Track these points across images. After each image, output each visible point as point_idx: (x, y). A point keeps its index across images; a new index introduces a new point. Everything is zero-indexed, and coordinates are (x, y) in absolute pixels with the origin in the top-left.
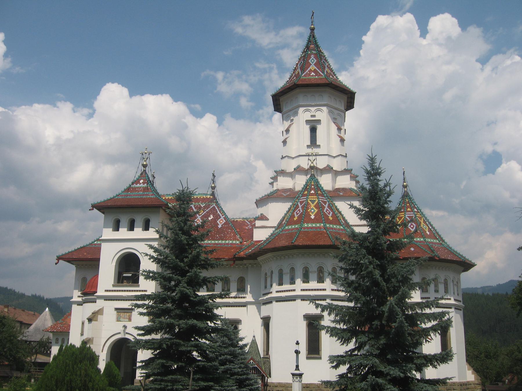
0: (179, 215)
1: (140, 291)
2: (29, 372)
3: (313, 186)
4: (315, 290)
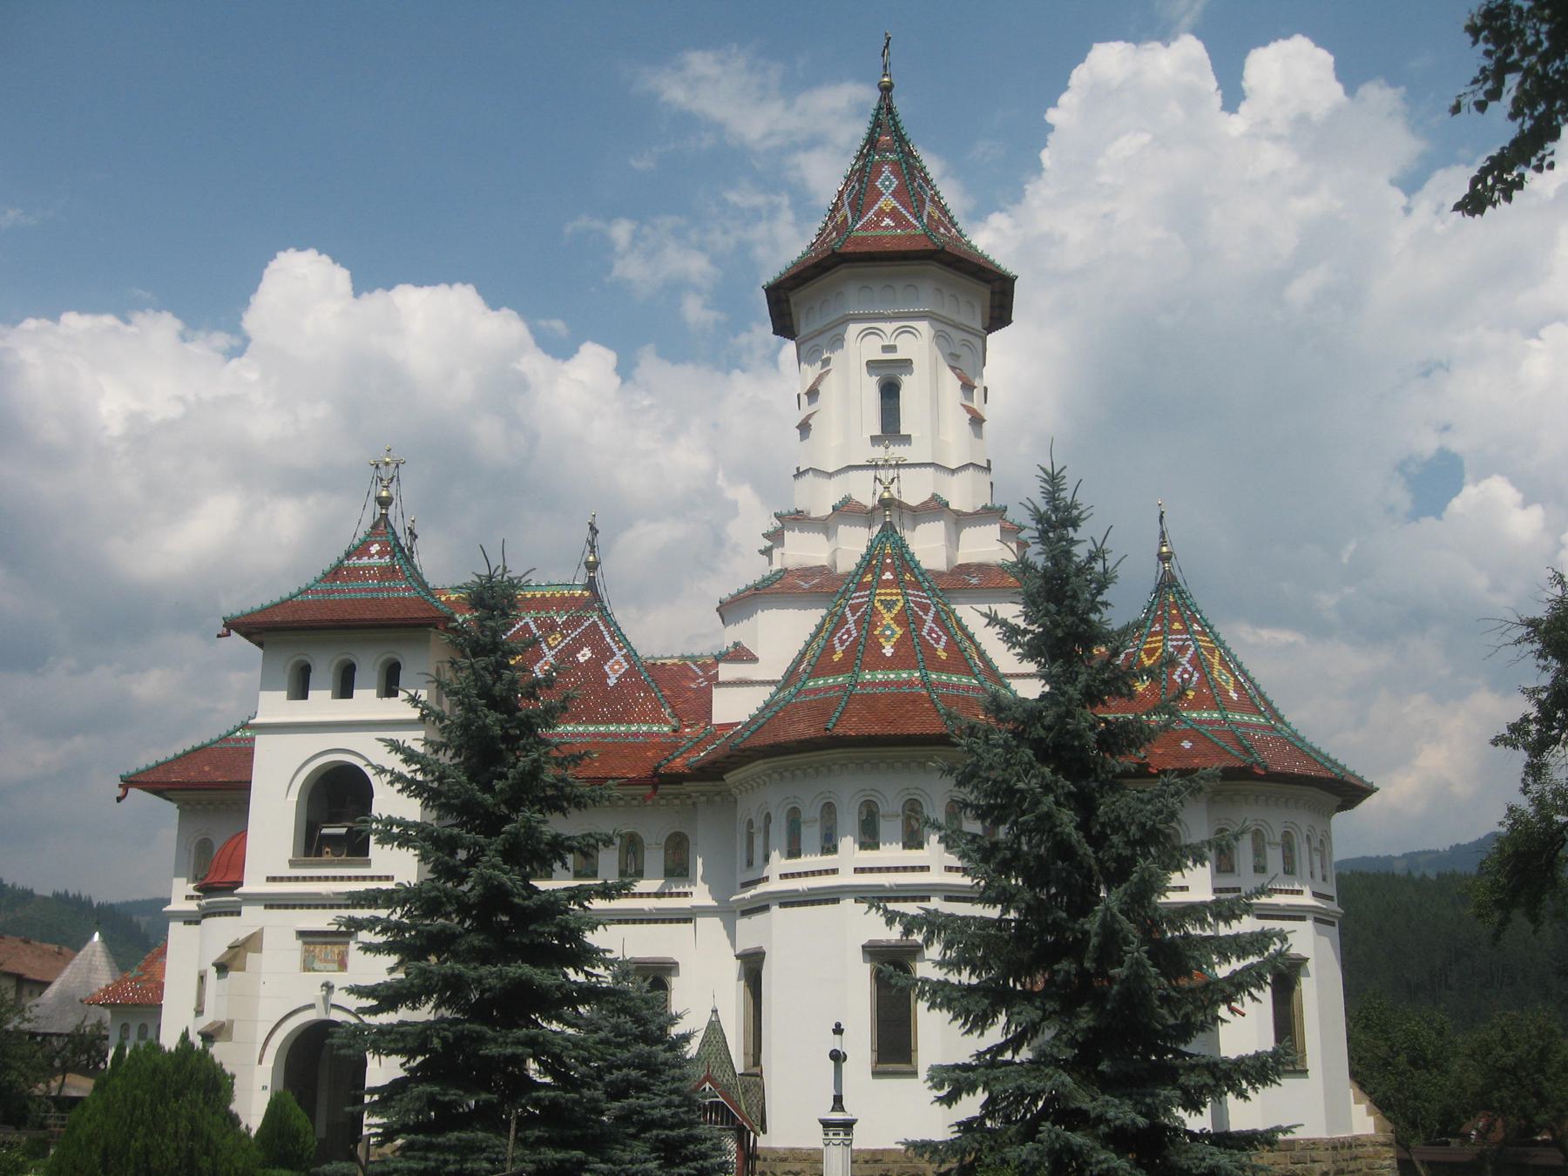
0: (478, 650)
1: (372, 878)
2: (43, 1127)
3: (886, 556)
4: (897, 869)
